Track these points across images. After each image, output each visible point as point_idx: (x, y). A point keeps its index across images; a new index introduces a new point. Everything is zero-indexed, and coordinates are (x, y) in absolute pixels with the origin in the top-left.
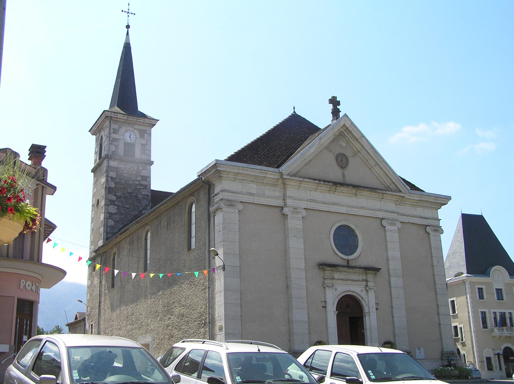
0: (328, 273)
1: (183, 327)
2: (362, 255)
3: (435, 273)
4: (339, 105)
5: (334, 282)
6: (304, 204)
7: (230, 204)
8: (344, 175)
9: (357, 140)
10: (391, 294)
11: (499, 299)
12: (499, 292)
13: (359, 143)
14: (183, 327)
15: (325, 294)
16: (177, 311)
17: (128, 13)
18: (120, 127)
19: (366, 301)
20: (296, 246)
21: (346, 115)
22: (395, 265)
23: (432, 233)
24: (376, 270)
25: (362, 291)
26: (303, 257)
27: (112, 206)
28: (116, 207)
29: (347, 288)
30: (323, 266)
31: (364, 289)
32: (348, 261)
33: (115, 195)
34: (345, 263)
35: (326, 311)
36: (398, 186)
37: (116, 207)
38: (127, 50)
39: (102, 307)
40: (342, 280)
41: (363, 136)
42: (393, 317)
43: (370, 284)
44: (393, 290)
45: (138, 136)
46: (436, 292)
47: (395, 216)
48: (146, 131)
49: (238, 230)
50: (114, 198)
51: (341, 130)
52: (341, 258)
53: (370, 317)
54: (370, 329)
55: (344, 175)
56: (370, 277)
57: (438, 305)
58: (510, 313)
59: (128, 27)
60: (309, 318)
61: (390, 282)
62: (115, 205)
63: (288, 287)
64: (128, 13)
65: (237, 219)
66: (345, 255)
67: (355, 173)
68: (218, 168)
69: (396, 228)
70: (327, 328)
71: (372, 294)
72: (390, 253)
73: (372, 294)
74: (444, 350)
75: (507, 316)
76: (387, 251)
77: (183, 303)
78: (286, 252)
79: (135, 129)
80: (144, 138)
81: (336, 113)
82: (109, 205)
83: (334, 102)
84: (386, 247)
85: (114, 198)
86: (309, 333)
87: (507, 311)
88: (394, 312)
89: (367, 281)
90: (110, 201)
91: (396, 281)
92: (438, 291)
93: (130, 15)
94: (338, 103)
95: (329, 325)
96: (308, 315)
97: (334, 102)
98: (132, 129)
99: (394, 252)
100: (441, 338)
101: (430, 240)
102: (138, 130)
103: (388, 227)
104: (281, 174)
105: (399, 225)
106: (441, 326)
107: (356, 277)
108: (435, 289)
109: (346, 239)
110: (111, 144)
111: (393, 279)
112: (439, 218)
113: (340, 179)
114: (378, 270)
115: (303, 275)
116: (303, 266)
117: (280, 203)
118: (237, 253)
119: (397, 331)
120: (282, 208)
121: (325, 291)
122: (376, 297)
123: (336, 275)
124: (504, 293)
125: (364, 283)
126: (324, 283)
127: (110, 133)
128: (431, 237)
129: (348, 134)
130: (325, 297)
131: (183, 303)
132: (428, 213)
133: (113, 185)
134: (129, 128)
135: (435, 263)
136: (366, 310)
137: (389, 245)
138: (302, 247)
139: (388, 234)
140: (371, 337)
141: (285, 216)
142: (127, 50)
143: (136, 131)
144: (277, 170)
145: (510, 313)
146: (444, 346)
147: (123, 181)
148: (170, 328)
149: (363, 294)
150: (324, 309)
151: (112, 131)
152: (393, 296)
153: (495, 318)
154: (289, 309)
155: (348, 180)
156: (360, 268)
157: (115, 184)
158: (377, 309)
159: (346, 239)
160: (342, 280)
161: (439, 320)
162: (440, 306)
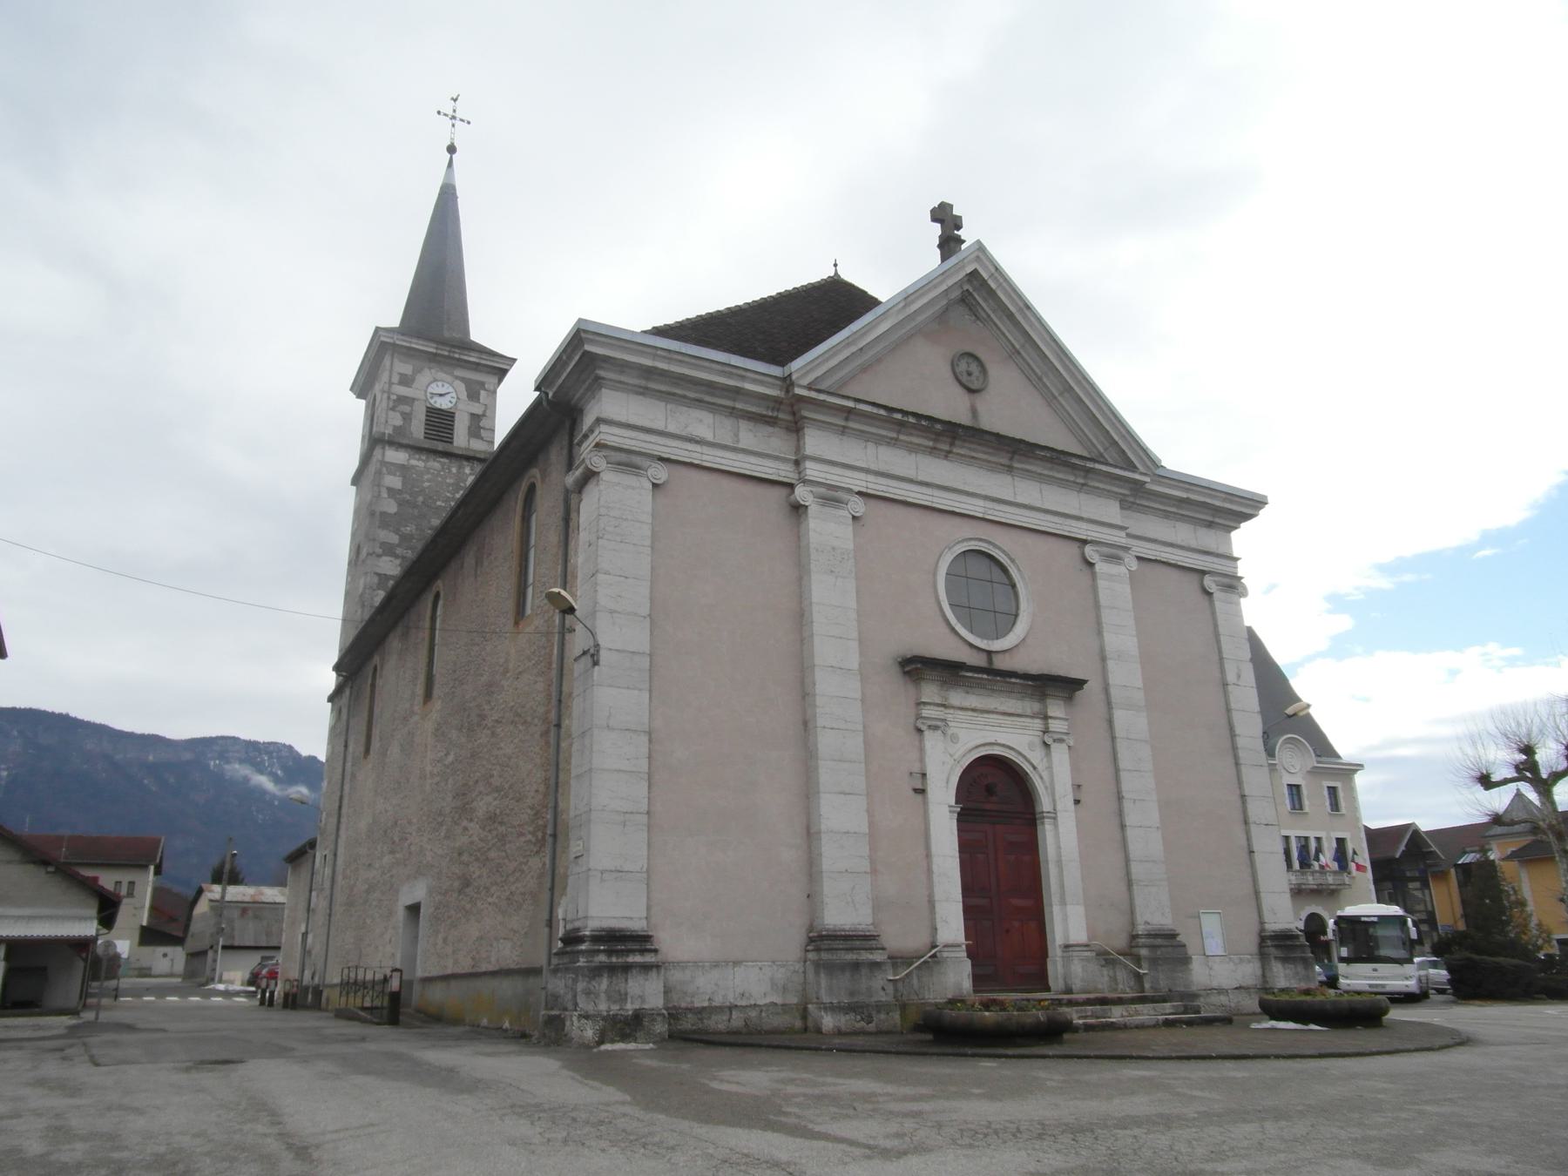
0: (930, 692)
1: (492, 854)
2: (1027, 642)
3: (1233, 706)
4: (959, 227)
5: (949, 715)
6: (858, 482)
7: (629, 462)
8: (974, 412)
9: (1011, 316)
10: (1115, 759)
11: (1294, 808)
12: (1295, 790)
13: (1017, 324)
14: (492, 854)
15: (922, 750)
16: (484, 804)
17: (454, 118)
18: (417, 371)
19: (1045, 774)
20: (833, 597)
21: (980, 247)
22: (1126, 676)
23: (1218, 595)
24: (1069, 687)
25: (1031, 746)
26: (855, 635)
27: (387, 558)
28: (398, 562)
29: (990, 737)
30: (916, 667)
31: (1037, 741)
32: (989, 653)
33: (397, 531)
34: (978, 660)
35: (925, 803)
36: (1130, 454)
37: (398, 562)
38: (447, 201)
39: (344, 810)
40: (974, 710)
41: (1028, 307)
42: (1123, 827)
43: (1055, 725)
44: (1121, 747)
45: (464, 395)
46: (1236, 757)
47: (1119, 538)
48: (482, 384)
49: (648, 542)
50: (394, 539)
51: (966, 287)
52: (971, 645)
53: (1056, 826)
54: (1059, 862)
55: (974, 412)
56: (1056, 709)
57: (1243, 797)
58: (1318, 839)
59: (452, 149)
60: (871, 824)
61: (1110, 722)
62: (397, 557)
63: (805, 723)
64: (454, 118)
65: (649, 508)
66: (983, 636)
67: (1010, 408)
68: (587, 347)
69: (1122, 569)
70: (928, 856)
71: (1060, 754)
72: (1112, 641)
73: (1060, 754)
74: (1267, 926)
75: (1313, 845)
76: (1100, 633)
77: (496, 781)
78: (801, 618)
79: (457, 378)
80: (478, 400)
81: (949, 243)
82: (379, 556)
83: (945, 217)
84: (1099, 623)
85: (394, 539)
86: (874, 871)
87: (1312, 834)
88: (1126, 810)
89: (1046, 718)
90: (383, 544)
91: (1131, 723)
92: (1241, 754)
93: (458, 123)
94: (957, 223)
95: (934, 849)
96: (870, 813)
97: (945, 217)
98: (449, 378)
99: (1122, 638)
100: (1257, 893)
101: (1213, 613)
102: (463, 379)
103: (1101, 567)
104: (787, 382)
105: (1134, 565)
106: (1258, 857)
107: (1011, 704)
108: (1234, 748)
109: (984, 580)
110: (393, 409)
111: (1119, 715)
112: (1236, 554)
113: (964, 418)
114: (1078, 684)
115: (854, 688)
116: (854, 662)
117: (784, 472)
118: (645, 611)
119: (1135, 869)
120: (791, 486)
121: (921, 741)
122: (1075, 769)
123: (957, 697)
124: (1305, 791)
125: (1038, 724)
126: (919, 717)
127: (391, 384)
128: (1218, 604)
129: (985, 300)
130: (922, 760)
131: (496, 781)
132: (1207, 539)
133: (391, 507)
134: (441, 375)
135: (1231, 678)
136: (1045, 804)
137: (1107, 617)
138: (854, 604)
139: (1101, 583)
140: (1062, 886)
141: (798, 509)
142: (447, 201)
143: (458, 383)
144: (776, 371)
145: (1318, 839)
146: (1267, 917)
147: (421, 499)
148: (465, 858)
149: (1036, 756)
150: (919, 797)
151: (396, 379)
152: (1122, 765)
153: (1287, 853)
154: (808, 792)
155: (987, 423)
156: (1026, 676)
157: (400, 505)
158: (1077, 802)
159: (984, 580)
160: (974, 710)
161: (1249, 839)
162: (1249, 800)
